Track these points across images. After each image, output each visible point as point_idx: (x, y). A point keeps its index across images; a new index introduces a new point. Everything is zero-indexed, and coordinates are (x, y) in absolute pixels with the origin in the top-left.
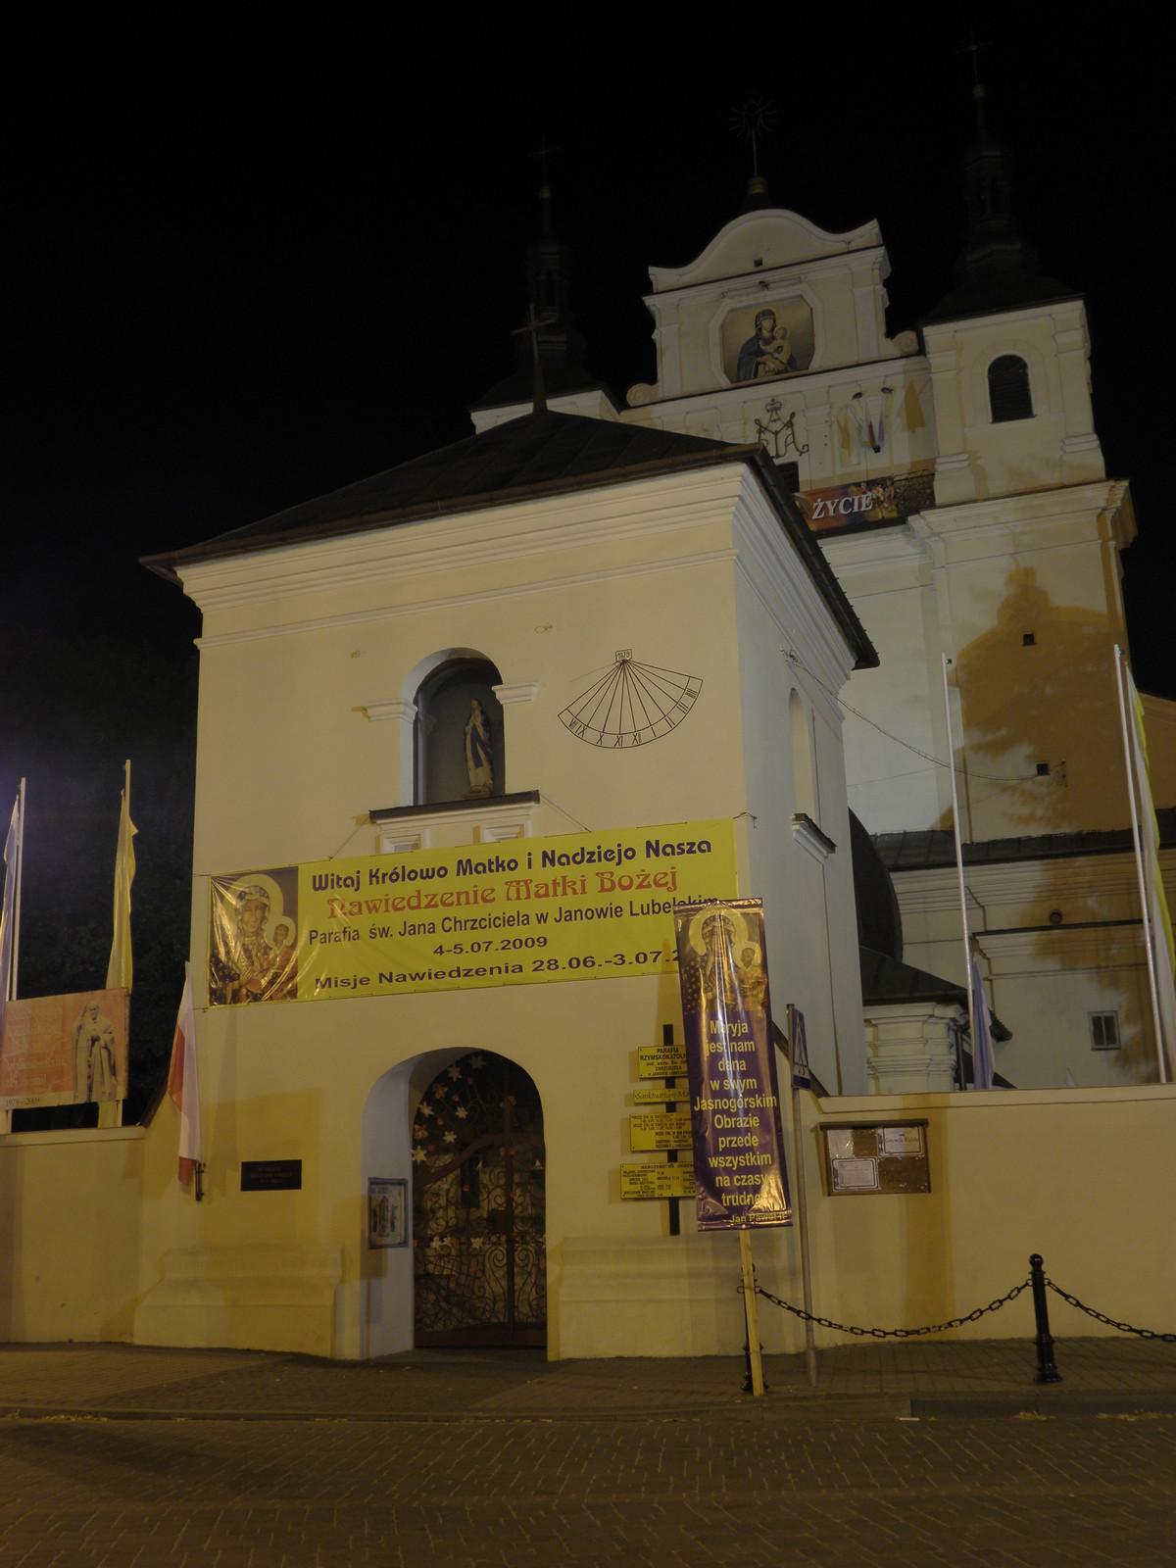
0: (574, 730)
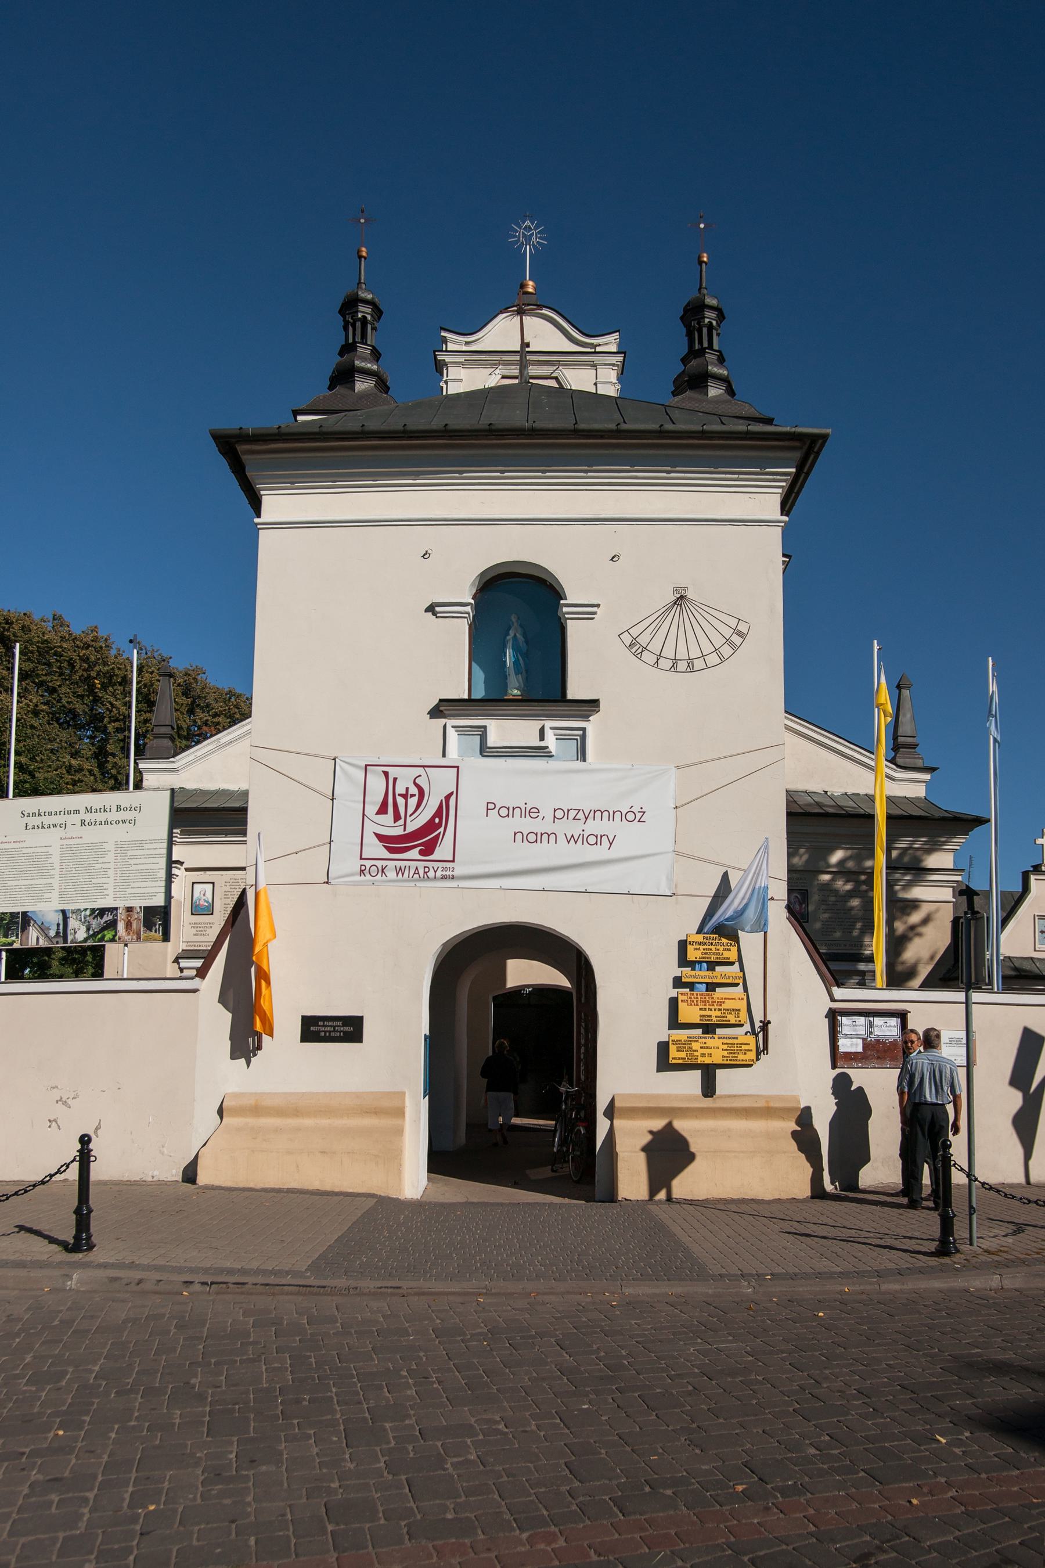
0: (633, 650)
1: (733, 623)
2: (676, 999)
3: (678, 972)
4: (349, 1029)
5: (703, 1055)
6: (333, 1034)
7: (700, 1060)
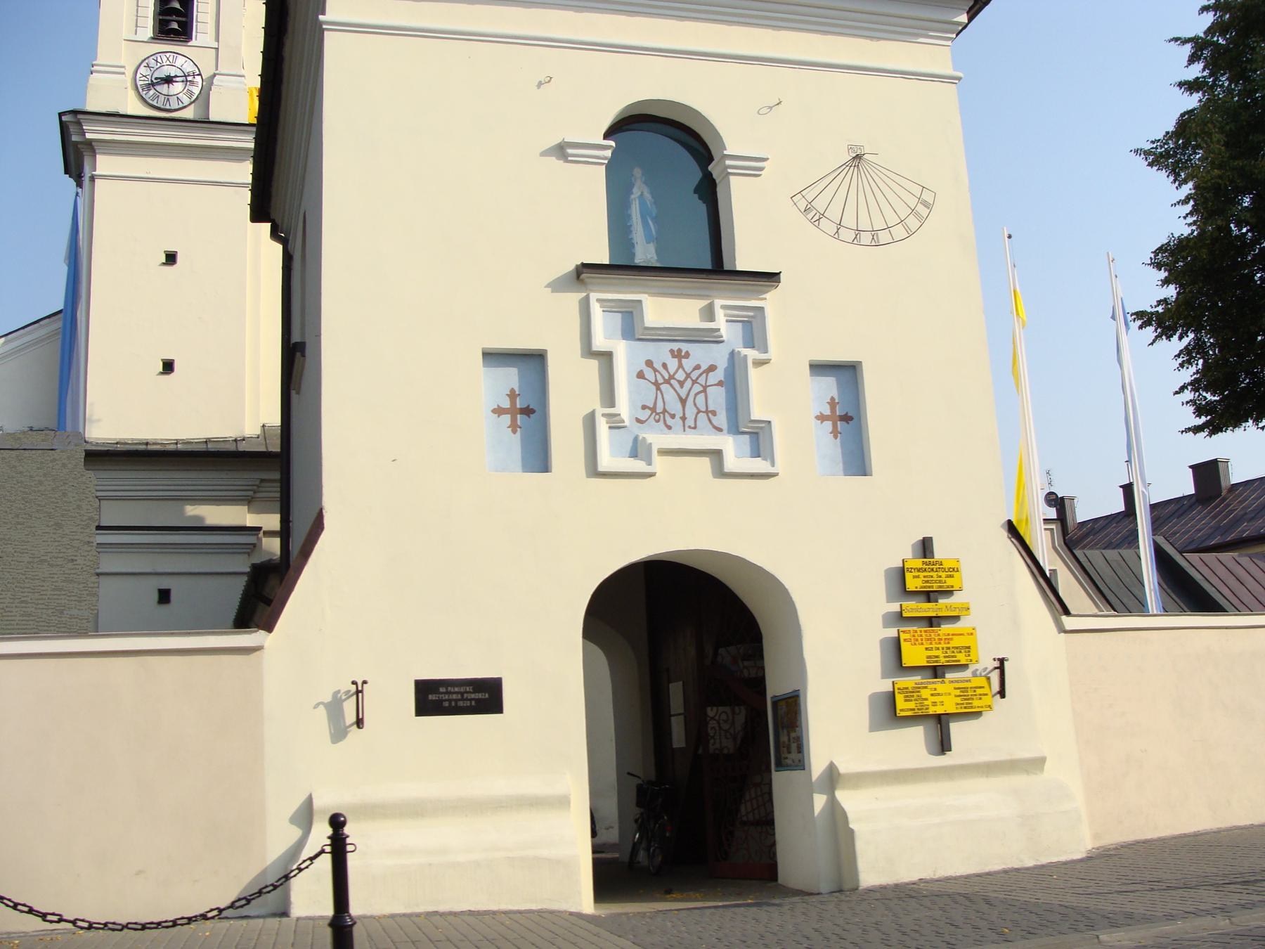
0: (810, 216)
1: (917, 190)
2: (898, 639)
3: (895, 607)
4: (483, 697)
5: (934, 704)
6: (461, 704)
7: (932, 710)
